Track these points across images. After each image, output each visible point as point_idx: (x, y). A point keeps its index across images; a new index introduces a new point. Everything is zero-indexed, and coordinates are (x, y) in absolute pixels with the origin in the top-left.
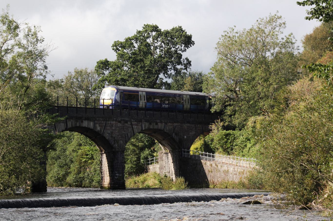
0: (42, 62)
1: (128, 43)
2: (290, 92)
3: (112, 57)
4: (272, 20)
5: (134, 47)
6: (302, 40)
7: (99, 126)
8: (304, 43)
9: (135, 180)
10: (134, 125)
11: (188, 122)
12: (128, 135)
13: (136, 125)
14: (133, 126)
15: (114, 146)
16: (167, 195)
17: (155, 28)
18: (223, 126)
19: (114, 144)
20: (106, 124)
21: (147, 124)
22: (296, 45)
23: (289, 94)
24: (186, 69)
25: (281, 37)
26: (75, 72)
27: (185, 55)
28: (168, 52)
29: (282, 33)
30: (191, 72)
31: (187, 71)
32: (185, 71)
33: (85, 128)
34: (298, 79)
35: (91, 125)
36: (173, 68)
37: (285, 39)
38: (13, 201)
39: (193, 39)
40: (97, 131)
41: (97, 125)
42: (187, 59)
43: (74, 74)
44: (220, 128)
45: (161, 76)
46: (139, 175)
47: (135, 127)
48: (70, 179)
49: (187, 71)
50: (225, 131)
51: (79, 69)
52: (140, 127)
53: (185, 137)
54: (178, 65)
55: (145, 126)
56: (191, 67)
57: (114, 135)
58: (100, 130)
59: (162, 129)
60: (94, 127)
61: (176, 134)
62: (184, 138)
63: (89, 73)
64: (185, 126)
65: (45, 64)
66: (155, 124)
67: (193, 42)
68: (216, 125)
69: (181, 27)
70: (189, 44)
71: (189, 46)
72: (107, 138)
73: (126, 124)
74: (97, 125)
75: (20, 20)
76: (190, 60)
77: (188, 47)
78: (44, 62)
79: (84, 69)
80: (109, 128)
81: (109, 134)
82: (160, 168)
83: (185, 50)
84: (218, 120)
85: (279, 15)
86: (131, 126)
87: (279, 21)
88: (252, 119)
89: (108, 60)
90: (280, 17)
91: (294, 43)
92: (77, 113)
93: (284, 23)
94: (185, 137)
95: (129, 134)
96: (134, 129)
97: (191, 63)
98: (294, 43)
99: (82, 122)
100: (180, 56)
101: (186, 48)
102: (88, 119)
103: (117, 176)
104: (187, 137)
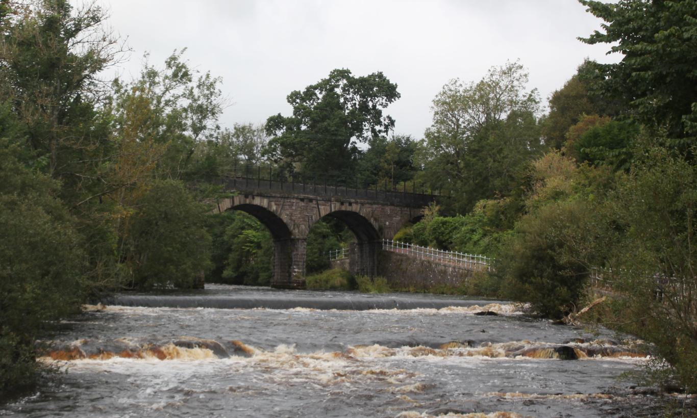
0: (214, 120)
1: (310, 93)
2: (534, 169)
3: (288, 112)
4: (508, 71)
5: (318, 99)
6: (548, 99)
7: (276, 204)
8: (550, 102)
9: (316, 279)
10: (321, 205)
11: (392, 204)
12: (312, 217)
13: (323, 205)
14: (320, 207)
15: (294, 231)
16: (203, 340)
17: (343, 74)
18: (439, 210)
19: (294, 229)
20: (284, 202)
21: (338, 204)
22: (541, 105)
23: (532, 172)
24: (386, 131)
25: (522, 94)
26: (235, 128)
27: (385, 113)
28: (364, 106)
29: (524, 88)
30: (395, 135)
31: (387, 134)
32: (384, 134)
33: (256, 206)
34: (546, 153)
35: (265, 203)
36: (370, 129)
37: (528, 96)
38: (195, 296)
39: (397, 90)
40: (272, 210)
41: (273, 203)
42: (389, 118)
43: (233, 131)
44: (435, 214)
45: (353, 139)
46: (321, 273)
47: (322, 207)
48: (227, 273)
49: (387, 134)
50: (442, 218)
51: (241, 124)
52: (328, 208)
53: (387, 223)
54: (377, 125)
55: (335, 208)
56: (394, 129)
57: (294, 218)
58: (277, 210)
59: (357, 211)
60: (268, 206)
61: (376, 220)
62: (385, 225)
63: (255, 131)
64: (388, 209)
65: (218, 123)
66: (348, 204)
67: (399, 94)
68: (430, 210)
69: (381, 73)
70: (392, 97)
71: (393, 100)
72: (285, 221)
73: (311, 204)
74: (273, 203)
75: (191, 68)
76: (393, 118)
77: (391, 101)
78: (217, 120)
79: (247, 124)
80: (288, 207)
81: (287, 215)
82: (350, 263)
83: (386, 106)
84: (433, 202)
85: (521, 64)
86: (316, 206)
87: (520, 72)
88: (482, 202)
89: (282, 115)
90: (521, 67)
91: (539, 102)
92: (247, 186)
93: (526, 75)
94: (387, 223)
95: (313, 217)
96: (321, 210)
97: (395, 123)
98: (539, 102)
99: (253, 198)
100: (379, 113)
101: (388, 103)
102: (261, 195)
103: (295, 272)
104: (389, 223)
